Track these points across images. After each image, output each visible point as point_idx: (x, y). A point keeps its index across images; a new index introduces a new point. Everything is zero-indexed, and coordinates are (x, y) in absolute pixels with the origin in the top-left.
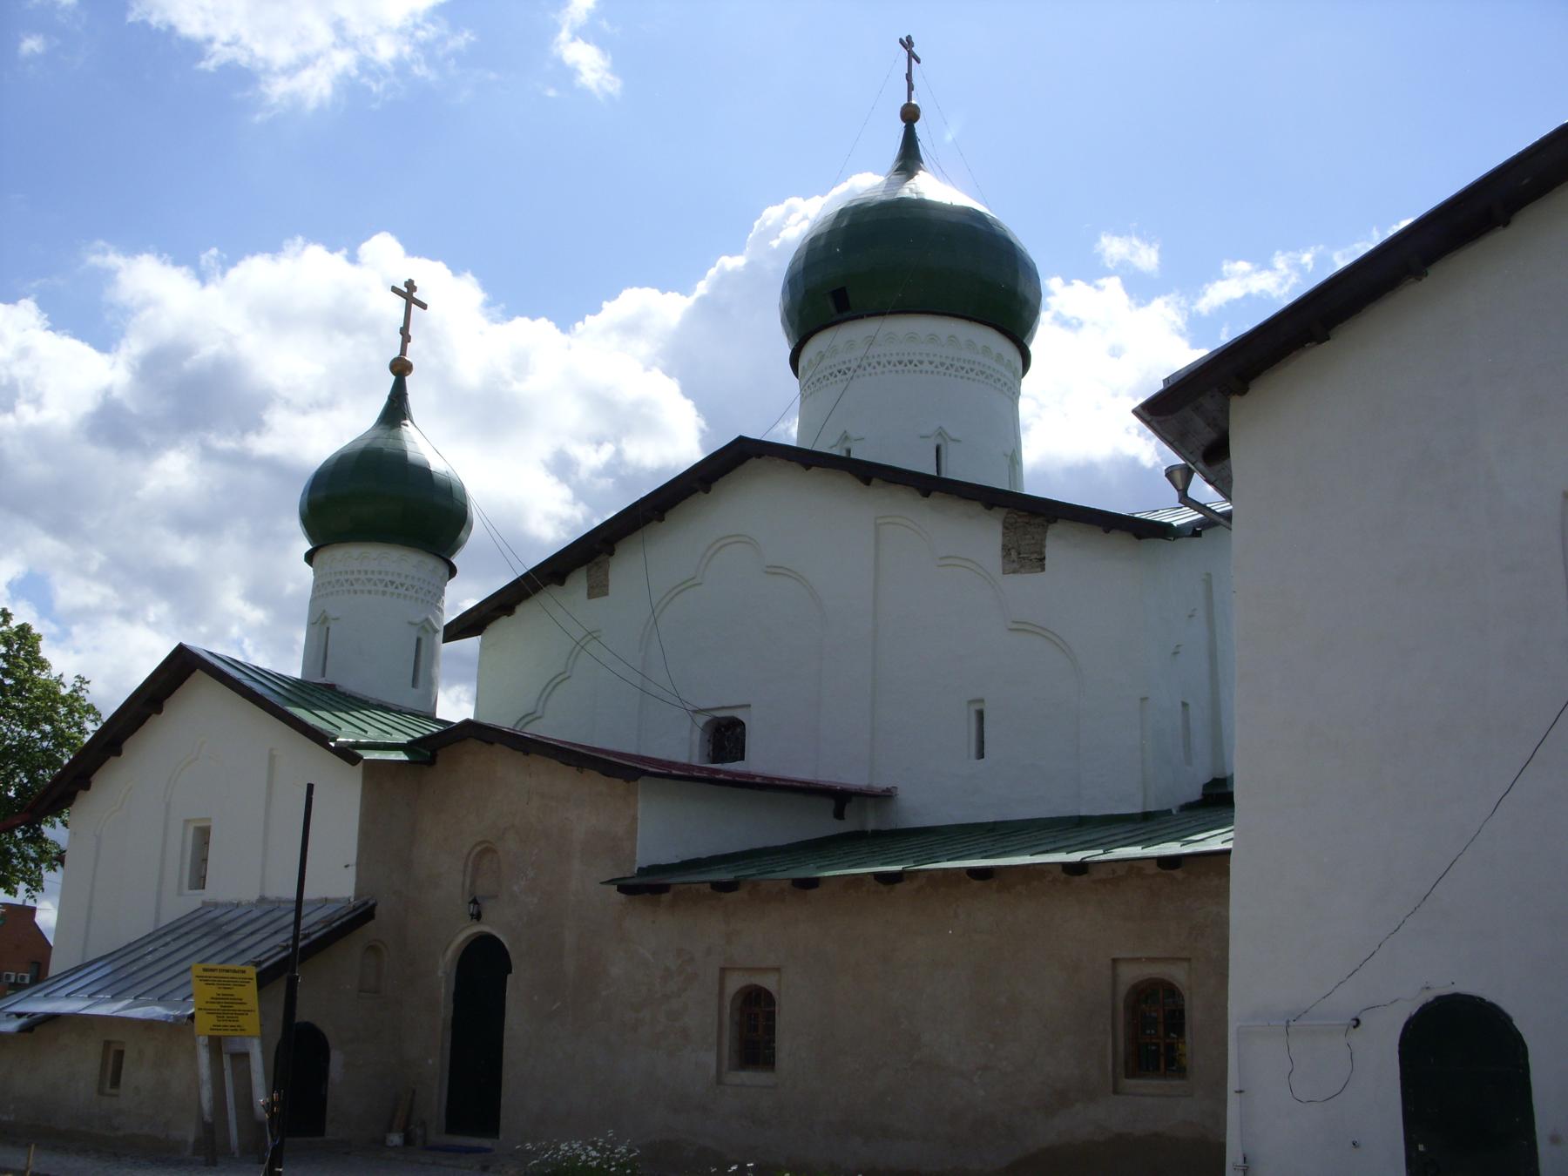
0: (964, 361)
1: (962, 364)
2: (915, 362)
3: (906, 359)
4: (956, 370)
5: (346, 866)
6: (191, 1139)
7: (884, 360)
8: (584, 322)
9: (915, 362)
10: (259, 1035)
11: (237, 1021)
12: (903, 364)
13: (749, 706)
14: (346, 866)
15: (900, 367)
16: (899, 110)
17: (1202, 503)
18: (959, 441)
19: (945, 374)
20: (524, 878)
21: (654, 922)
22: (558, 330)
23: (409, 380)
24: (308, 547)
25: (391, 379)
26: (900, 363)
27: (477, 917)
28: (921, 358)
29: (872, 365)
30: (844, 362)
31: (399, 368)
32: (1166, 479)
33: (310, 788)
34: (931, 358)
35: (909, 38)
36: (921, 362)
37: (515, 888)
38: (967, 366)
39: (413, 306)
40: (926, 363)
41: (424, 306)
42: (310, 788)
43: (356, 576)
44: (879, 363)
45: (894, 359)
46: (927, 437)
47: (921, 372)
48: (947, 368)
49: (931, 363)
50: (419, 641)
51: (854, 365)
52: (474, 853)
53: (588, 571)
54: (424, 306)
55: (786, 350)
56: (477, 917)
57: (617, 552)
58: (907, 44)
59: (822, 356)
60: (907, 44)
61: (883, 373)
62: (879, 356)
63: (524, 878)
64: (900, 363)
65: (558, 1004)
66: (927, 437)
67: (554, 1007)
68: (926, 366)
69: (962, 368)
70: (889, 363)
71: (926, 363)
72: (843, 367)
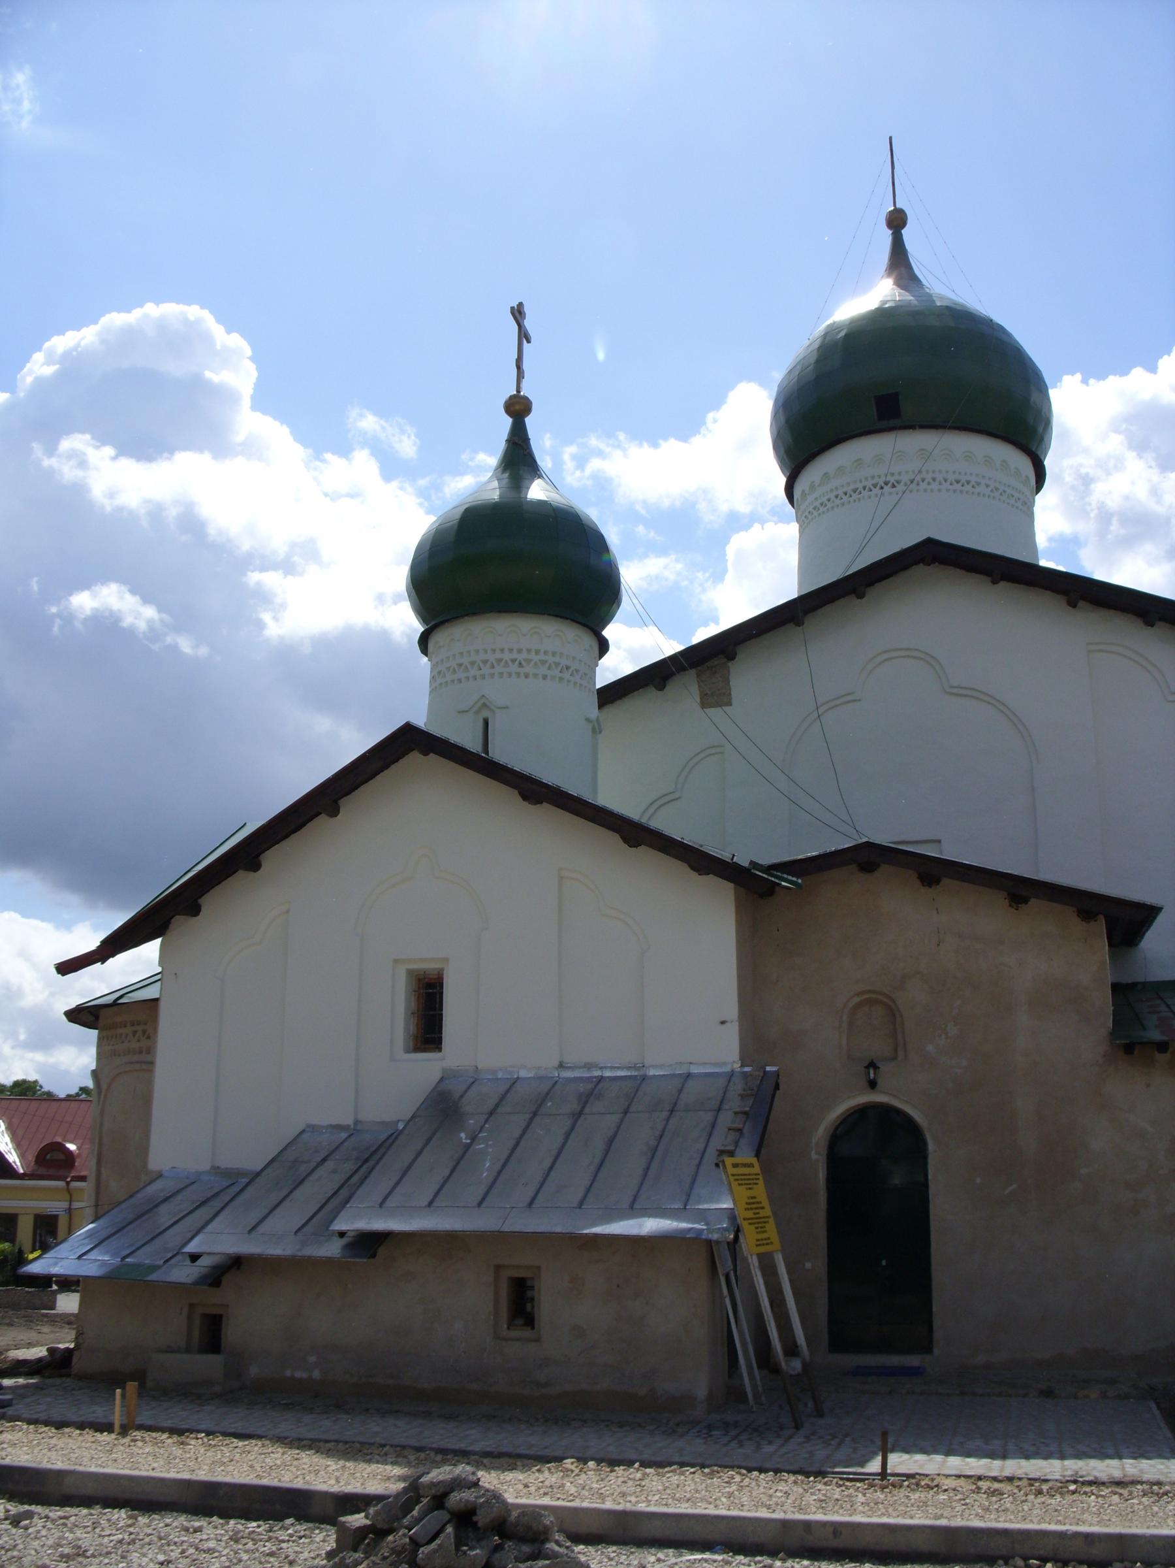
0: (486, 651)
2: (963, 481)
3: (963, 479)
5: (723, 1023)
6: (702, 1392)
7: (940, 478)
10: (780, 1248)
11: (765, 1232)
12: (961, 484)
14: (723, 1023)
15: (958, 487)
18: (507, 707)
20: (943, 1036)
21: (1148, 1086)
23: (529, 421)
25: (508, 421)
26: (958, 482)
27: (872, 1084)
29: (938, 480)
31: (517, 407)
33: (891, 138)
35: (520, 305)
36: (978, 484)
37: (930, 1048)
42: (891, 138)
43: (524, 655)
44: (934, 480)
45: (952, 477)
46: (467, 711)
47: (979, 494)
48: (992, 491)
49: (987, 486)
51: (905, 479)
52: (851, 1005)
53: (698, 675)
55: (782, 480)
56: (872, 1084)
57: (667, 688)
58: (518, 313)
59: (813, 487)
60: (518, 313)
62: (947, 472)
63: (943, 1036)
64: (958, 482)
65: (1014, 1186)
66: (467, 711)
67: (1007, 1191)
70: (946, 481)
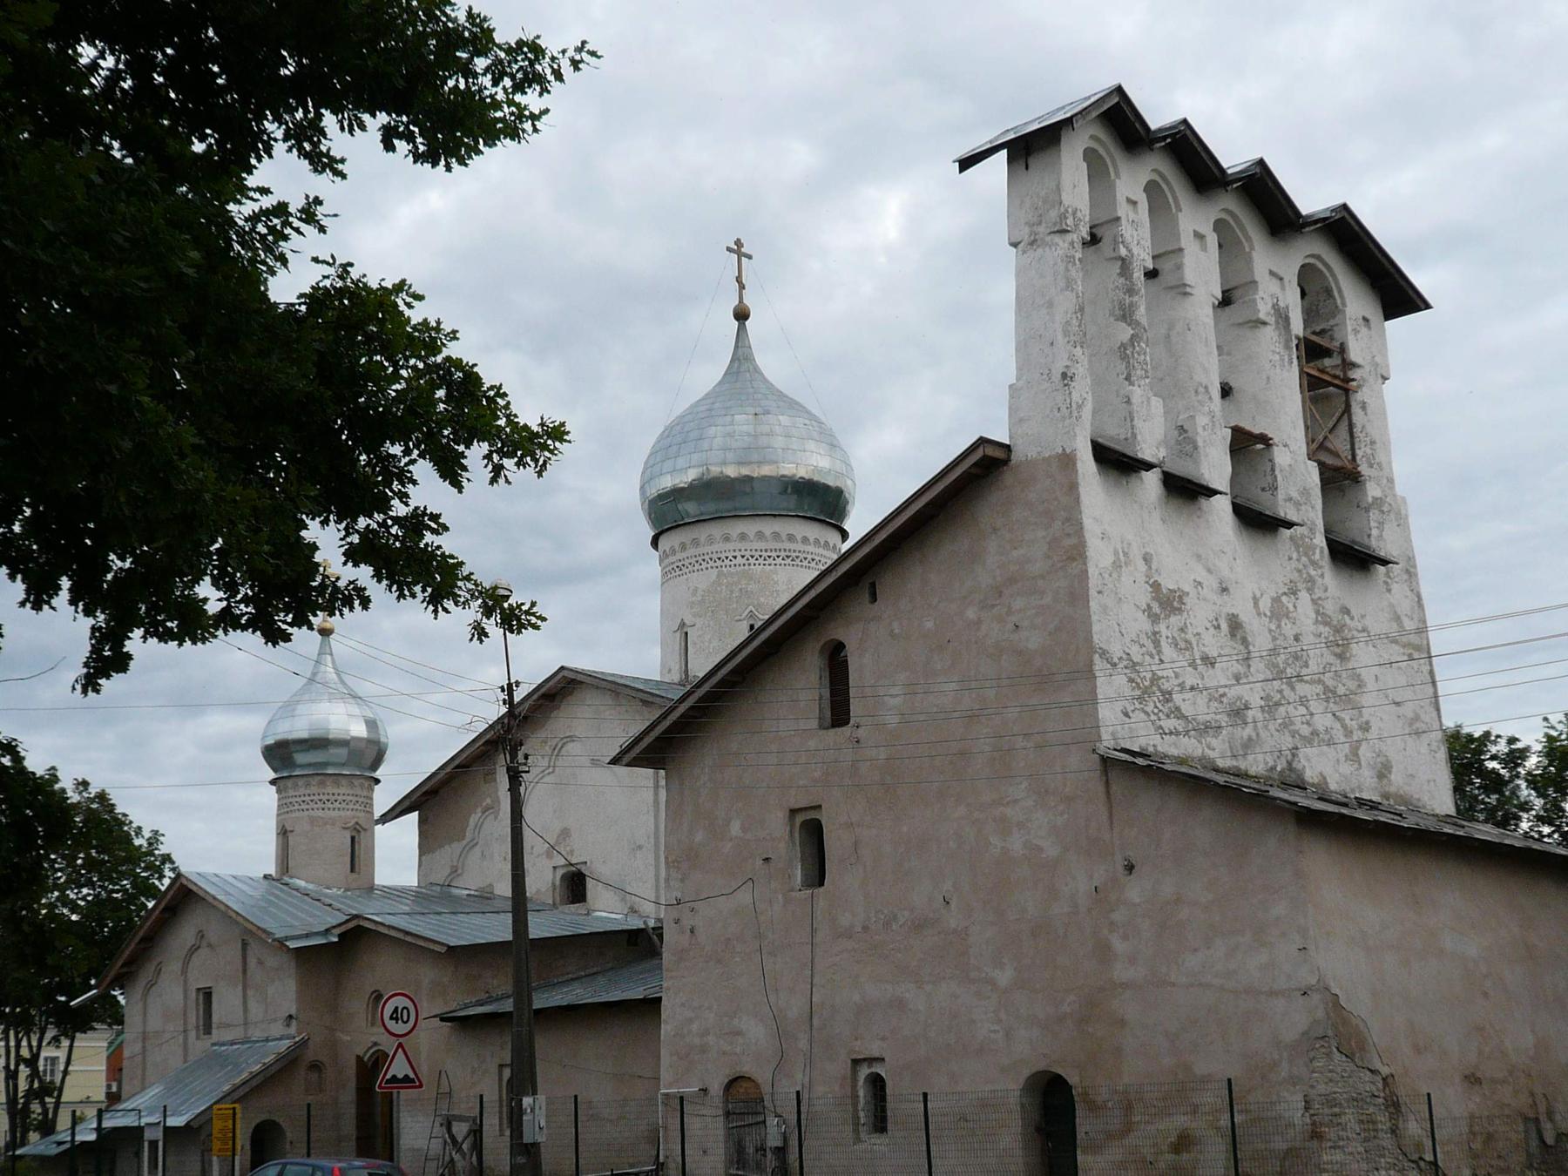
1: (805, 555)
4: (793, 560)
7: (707, 558)
8: (180, 645)
9: (730, 558)
13: (820, 806)
16: (261, 754)
17: (496, 710)
19: (707, 569)
22: (382, 145)
24: (272, 775)
28: (735, 554)
30: (766, 551)
32: (386, 825)
34: (743, 553)
38: (774, 554)
39: (400, 1050)
40: (739, 557)
41: (750, 257)
50: (353, 839)
54: (750, 257)
61: (707, 569)
68: (740, 560)
69: (769, 557)
71: (739, 557)
72: (680, 564)
